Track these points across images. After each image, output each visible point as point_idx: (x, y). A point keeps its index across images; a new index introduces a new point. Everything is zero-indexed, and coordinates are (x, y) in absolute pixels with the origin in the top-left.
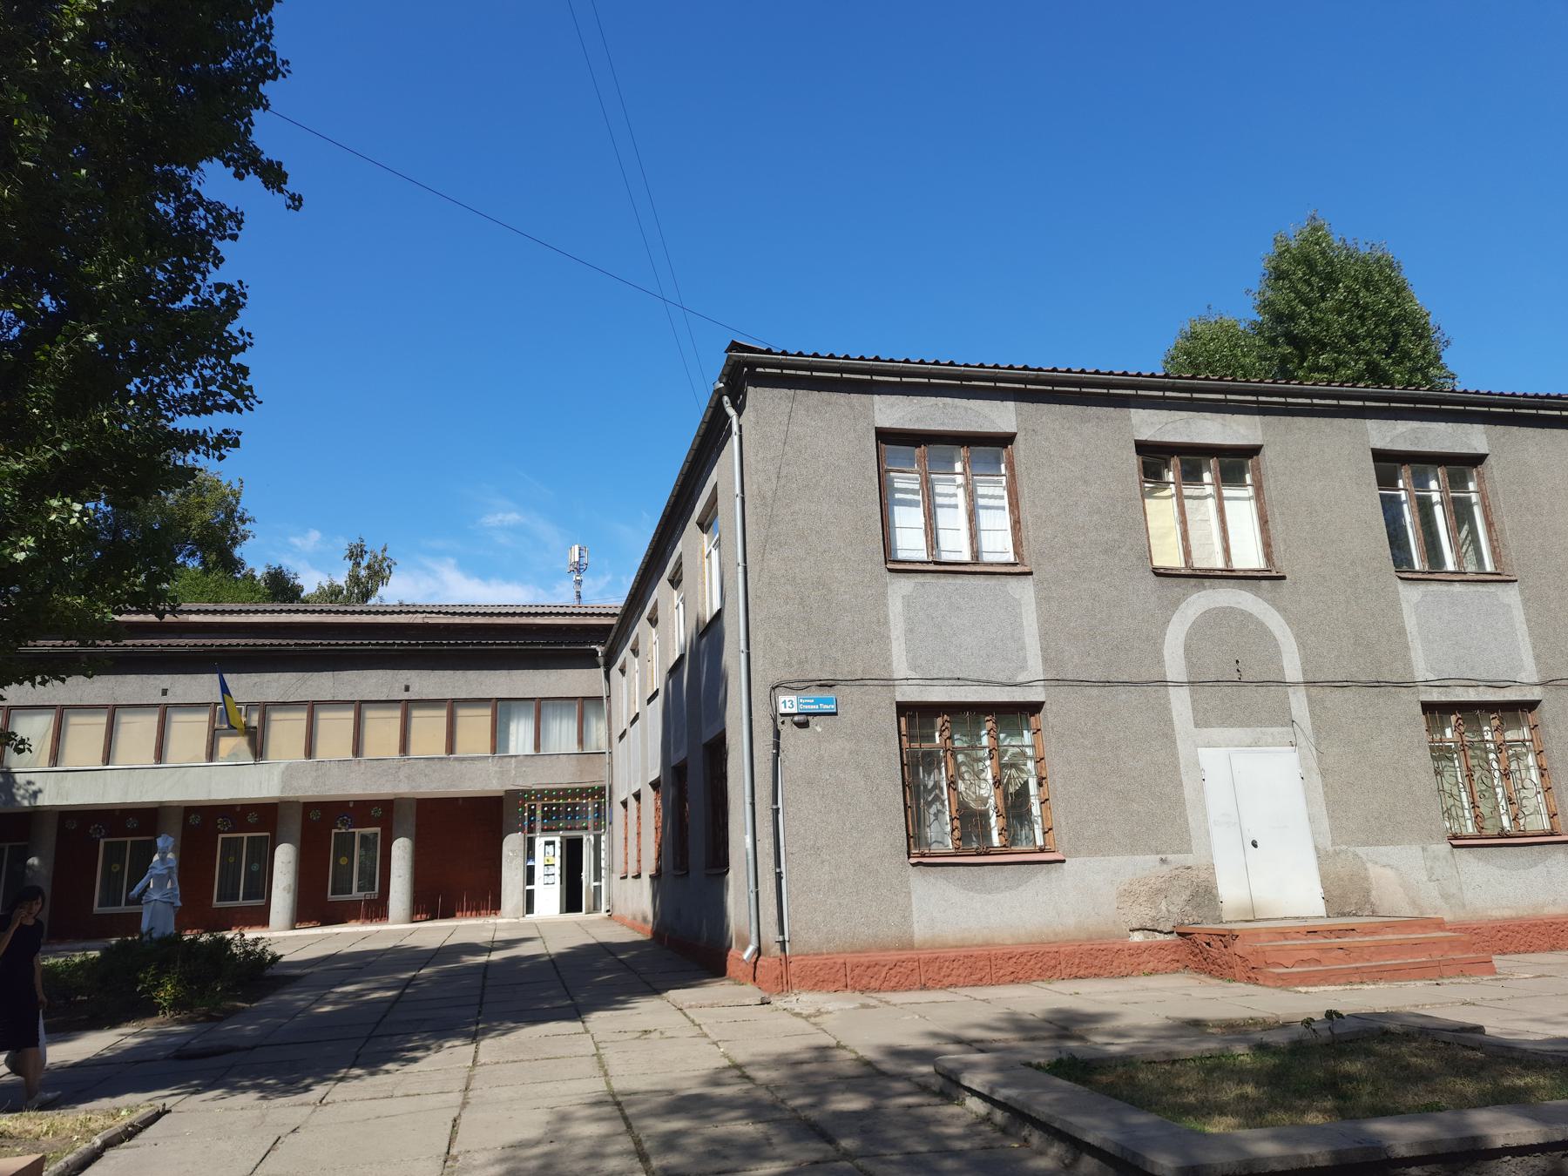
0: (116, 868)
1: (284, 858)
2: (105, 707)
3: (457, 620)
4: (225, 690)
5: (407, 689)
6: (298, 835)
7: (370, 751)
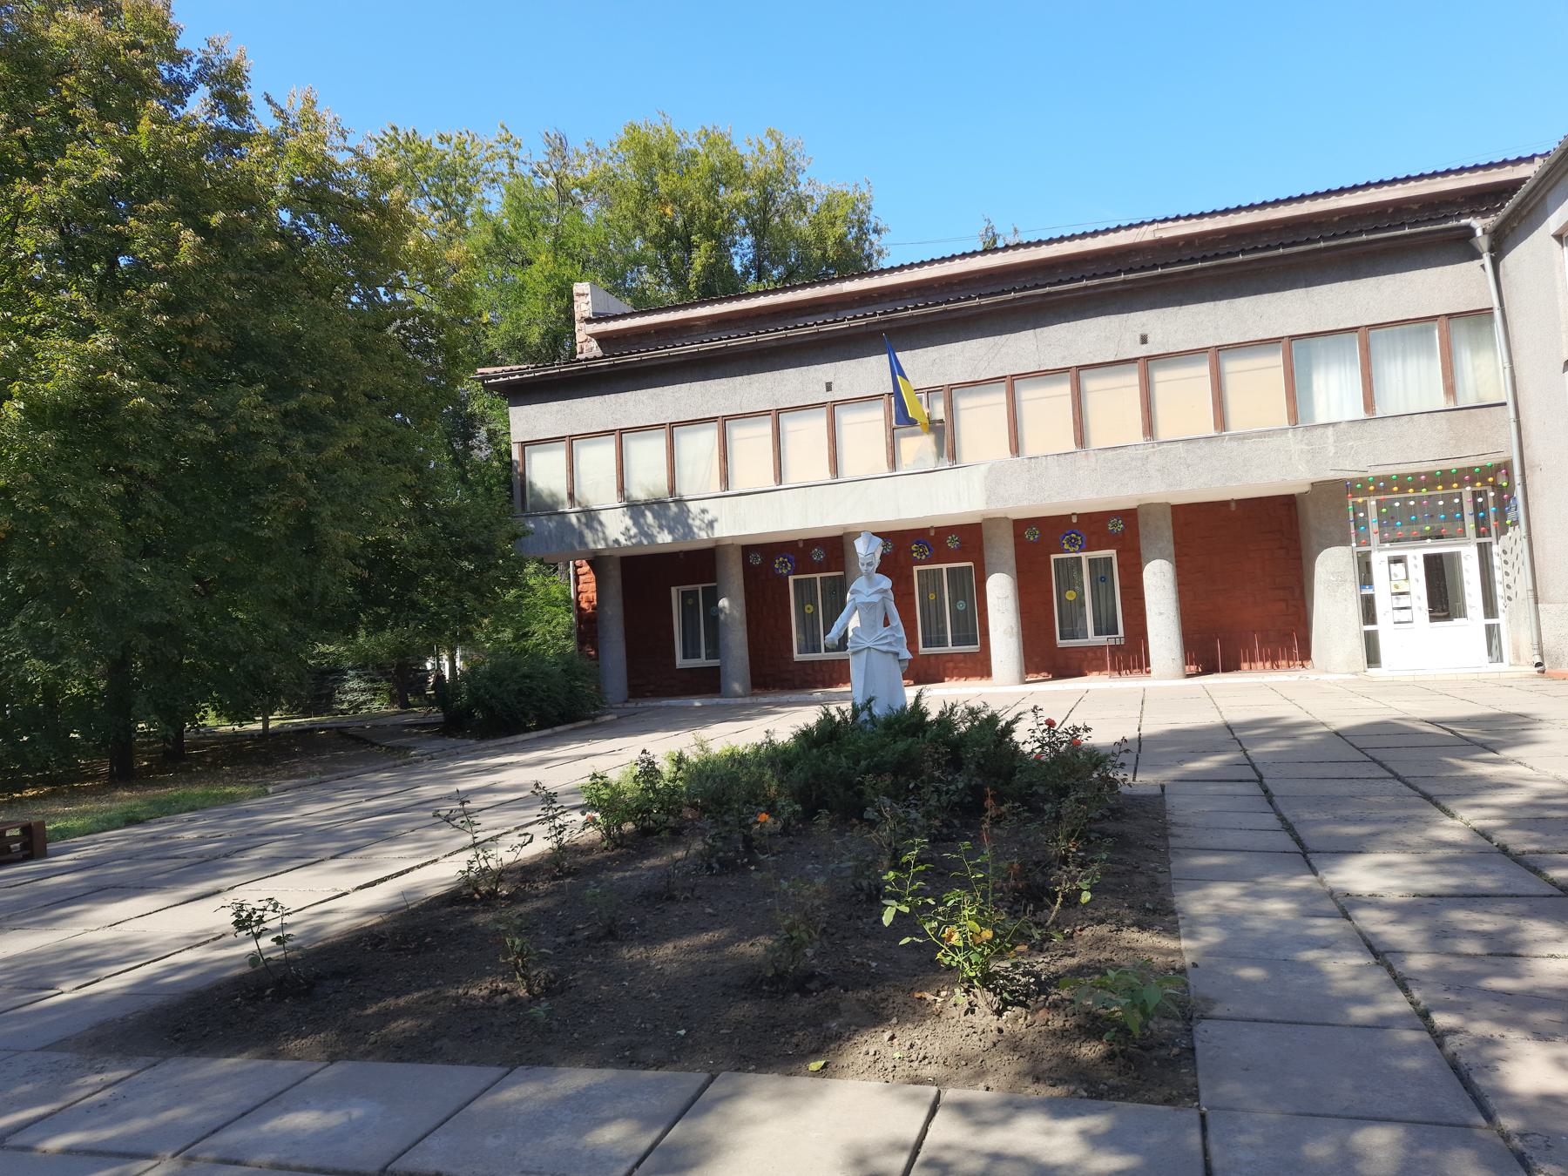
0: (809, 609)
1: (1000, 591)
2: (767, 413)
3: (1208, 225)
4: (897, 370)
5: (1144, 340)
6: (1012, 562)
7: (1099, 435)
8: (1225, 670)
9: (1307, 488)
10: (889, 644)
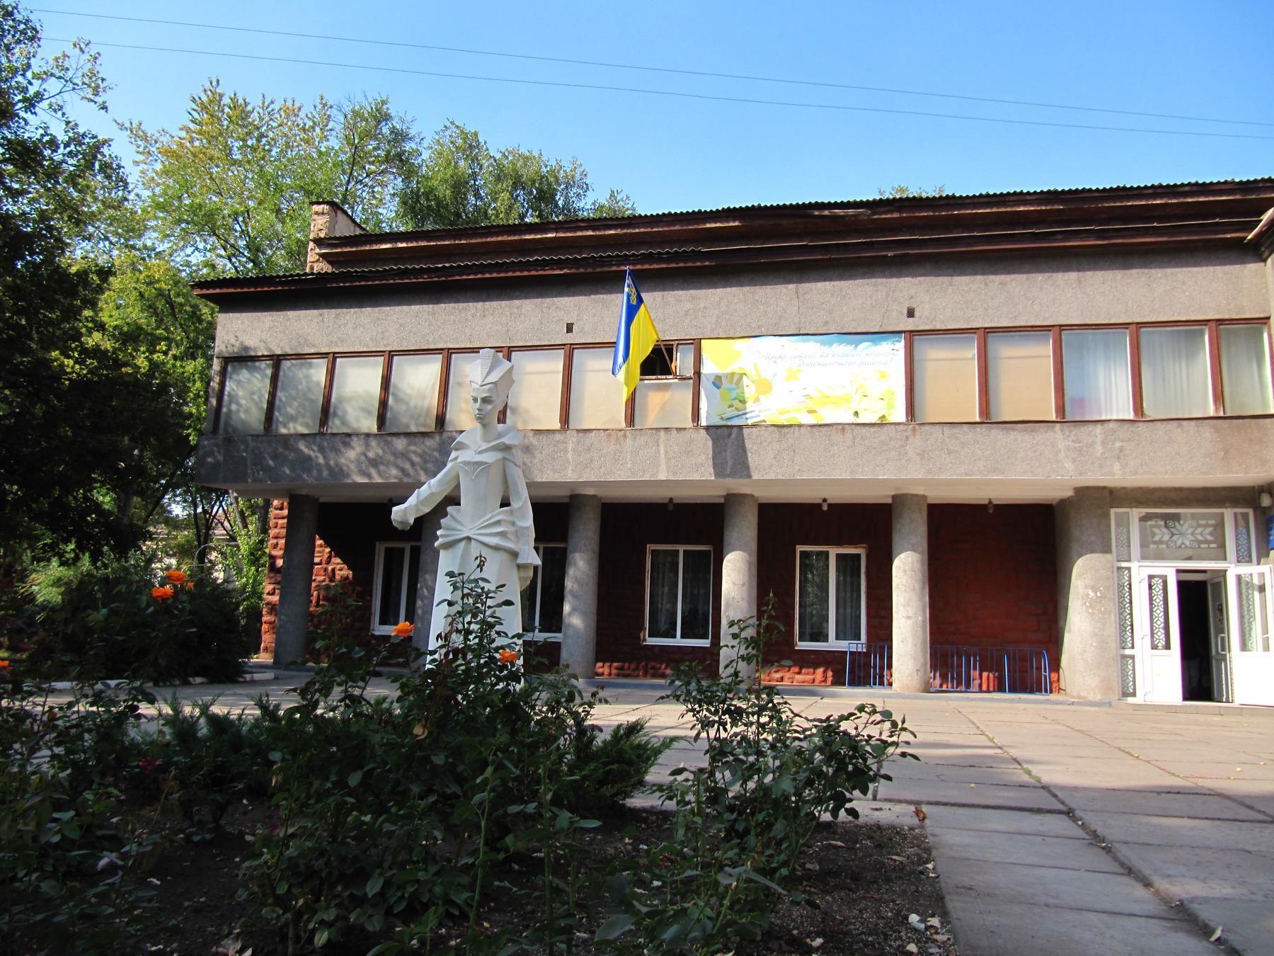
5: (911, 313)
9: (1070, 493)
10: (502, 534)
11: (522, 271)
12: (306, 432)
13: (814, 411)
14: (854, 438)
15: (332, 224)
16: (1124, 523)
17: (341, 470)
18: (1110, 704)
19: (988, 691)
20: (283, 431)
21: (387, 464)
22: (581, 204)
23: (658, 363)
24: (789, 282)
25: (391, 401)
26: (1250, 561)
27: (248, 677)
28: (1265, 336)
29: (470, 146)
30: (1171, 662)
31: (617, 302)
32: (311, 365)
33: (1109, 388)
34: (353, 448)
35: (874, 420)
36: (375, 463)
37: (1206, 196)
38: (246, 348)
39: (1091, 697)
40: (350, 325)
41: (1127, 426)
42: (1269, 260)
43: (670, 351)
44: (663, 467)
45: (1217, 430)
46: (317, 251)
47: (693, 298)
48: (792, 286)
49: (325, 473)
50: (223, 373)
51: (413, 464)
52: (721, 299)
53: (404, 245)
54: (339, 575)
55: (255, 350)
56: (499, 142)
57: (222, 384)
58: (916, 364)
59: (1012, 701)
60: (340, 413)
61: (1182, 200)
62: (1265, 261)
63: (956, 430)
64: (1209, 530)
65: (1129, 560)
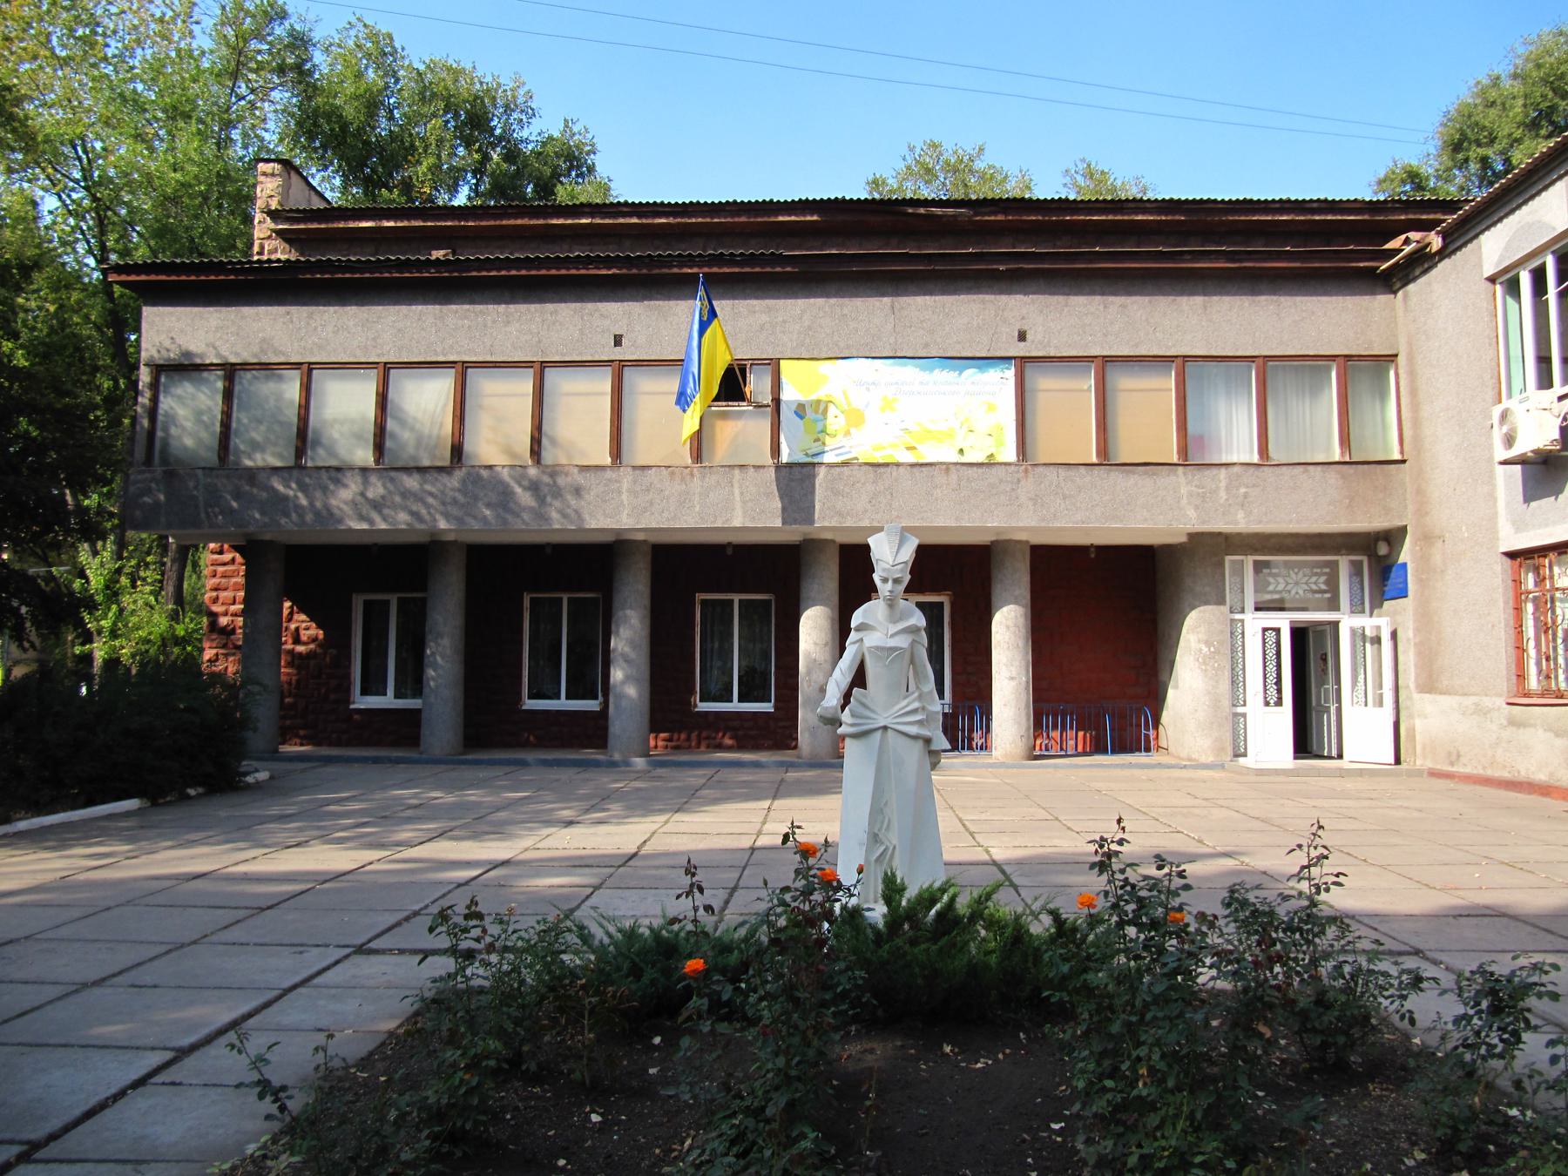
1: (628, 640)
5: (1022, 337)
8: (1114, 752)
9: (1184, 539)
11: (558, 269)
12: (279, 464)
13: (913, 448)
14: (959, 480)
15: (285, 190)
16: (1239, 571)
17: (332, 514)
18: (1223, 766)
19: (1084, 754)
20: (248, 463)
21: (394, 507)
22: (525, 134)
23: (732, 386)
24: (883, 295)
25: (391, 425)
26: (1363, 612)
27: (250, 779)
28: (1392, 373)
29: (383, 52)
30: (1283, 718)
31: (686, 311)
32: (280, 378)
33: (1234, 429)
34: (345, 486)
35: (981, 459)
36: (377, 505)
37: (1335, 213)
38: (187, 354)
39: (1204, 759)
40: (330, 328)
41: (1252, 469)
42: (1400, 293)
43: (743, 370)
44: (739, 512)
45: (1343, 477)
46: (273, 226)
47: (770, 309)
48: (886, 300)
49: (309, 517)
50: (155, 386)
51: (428, 506)
52: (803, 312)
53: (391, 224)
54: (304, 635)
55: (201, 356)
56: (420, 50)
57: (155, 400)
58: (1027, 395)
59: (1122, 766)
60: (324, 441)
61: (1309, 217)
62: (1395, 293)
63: (1072, 472)
64: (1323, 579)
65: (1243, 611)
